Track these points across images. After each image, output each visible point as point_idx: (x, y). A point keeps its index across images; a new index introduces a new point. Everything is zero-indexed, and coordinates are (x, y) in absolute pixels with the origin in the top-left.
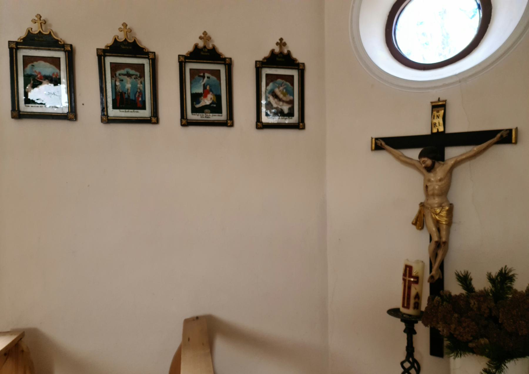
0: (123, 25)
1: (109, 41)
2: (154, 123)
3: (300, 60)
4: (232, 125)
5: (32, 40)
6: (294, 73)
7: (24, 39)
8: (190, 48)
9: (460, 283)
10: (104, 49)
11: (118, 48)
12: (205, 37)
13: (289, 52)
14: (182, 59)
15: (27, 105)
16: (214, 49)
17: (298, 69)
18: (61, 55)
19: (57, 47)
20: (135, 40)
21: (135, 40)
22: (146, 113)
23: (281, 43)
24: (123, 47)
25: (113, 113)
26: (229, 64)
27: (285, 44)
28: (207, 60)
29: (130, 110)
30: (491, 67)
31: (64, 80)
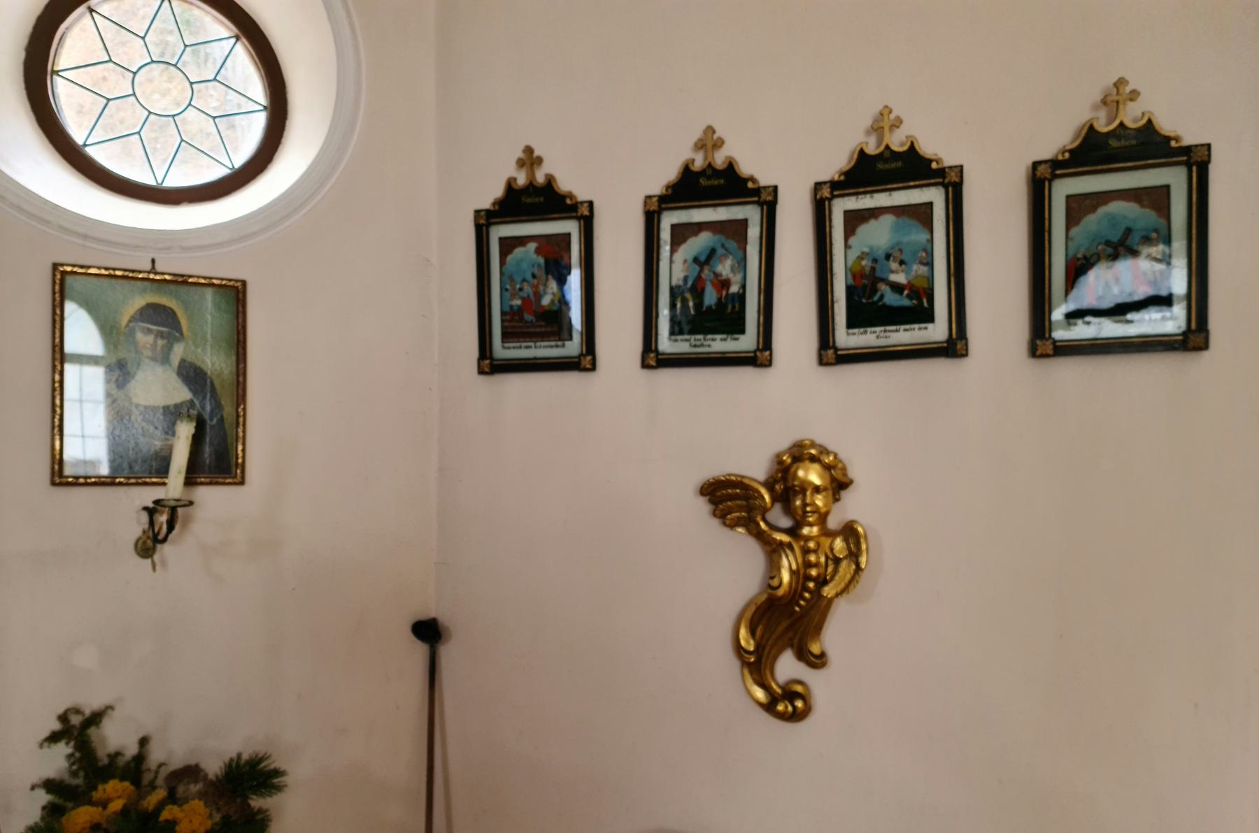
0: (524, 151)
1: (671, 173)
2: (586, 370)
3: (582, 194)
4: (593, 368)
5: (1092, 151)
6: (934, 196)
7: (848, 174)
8: (498, 191)
9: (245, 757)
10: (487, 211)
11: (868, 171)
12: (710, 141)
13: (550, 180)
14: (953, 177)
15: (851, 331)
16: (731, 167)
17: (760, 204)
18: (934, 196)
19: (566, 211)
20: (1150, 121)
21: (1150, 121)
22: (747, 342)
23: (530, 160)
24: (529, 200)
25: (845, 338)
26: (952, 183)
27: (539, 160)
28: (738, 197)
29: (903, 327)
30: (34, 223)
31: (1179, 244)
